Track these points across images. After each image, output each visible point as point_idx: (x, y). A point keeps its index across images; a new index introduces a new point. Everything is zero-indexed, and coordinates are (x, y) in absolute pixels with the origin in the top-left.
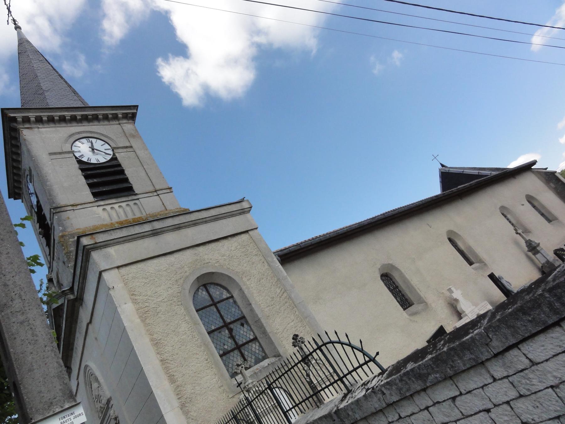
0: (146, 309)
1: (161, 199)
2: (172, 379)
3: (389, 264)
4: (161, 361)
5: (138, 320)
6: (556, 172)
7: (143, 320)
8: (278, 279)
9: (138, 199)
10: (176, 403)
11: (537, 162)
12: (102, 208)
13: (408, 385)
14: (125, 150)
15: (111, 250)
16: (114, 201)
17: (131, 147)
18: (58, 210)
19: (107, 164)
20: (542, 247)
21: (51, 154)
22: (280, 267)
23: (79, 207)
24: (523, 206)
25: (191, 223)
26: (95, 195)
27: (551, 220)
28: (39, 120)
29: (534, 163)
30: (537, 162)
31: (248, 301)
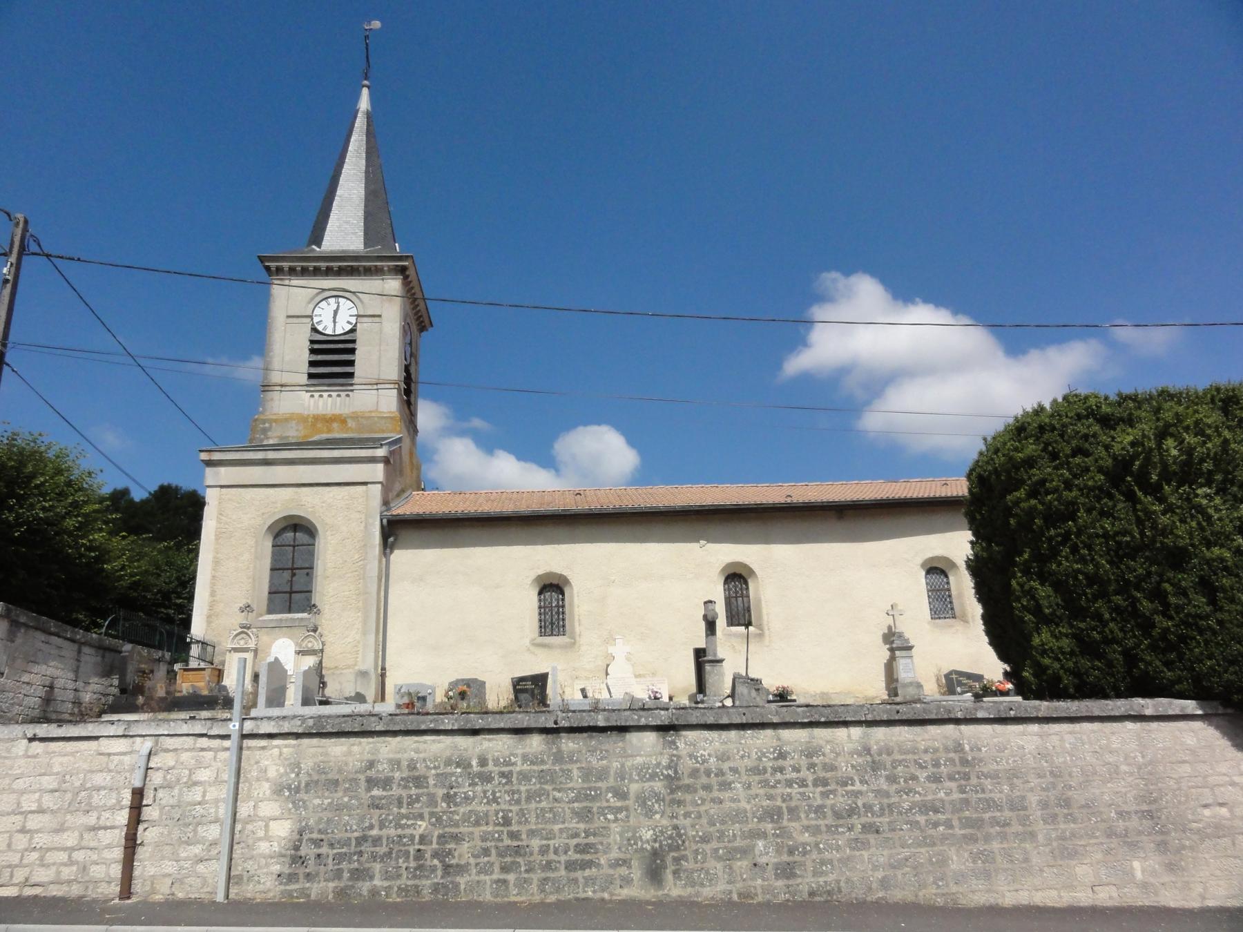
0: (224, 530)
2: (213, 594)
4: (213, 577)
5: (213, 537)
7: (217, 539)
8: (365, 545)
10: (205, 611)
13: (1144, 853)
14: (370, 319)
15: (222, 470)
18: (267, 388)
19: (342, 338)
20: (913, 655)
21: (288, 317)
23: (288, 388)
27: (957, 614)
28: (292, 271)
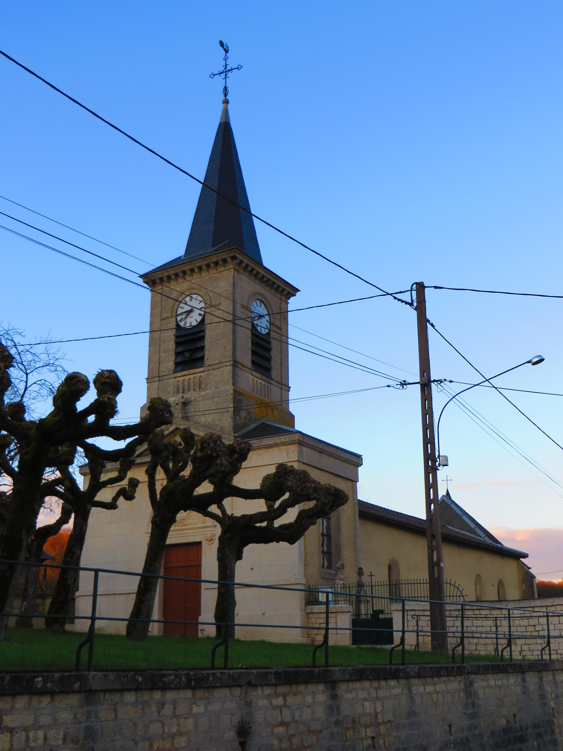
1: (281, 393)
3: (396, 561)
6: (535, 577)
9: (271, 384)
11: (528, 557)
12: (252, 377)
16: (259, 376)
17: (281, 329)
22: (358, 519)
24: (492, 586)
25: (335, 456)
26: (253, 363)
29: (525, 556)
30: (528, 557)
31: (340, 529)
